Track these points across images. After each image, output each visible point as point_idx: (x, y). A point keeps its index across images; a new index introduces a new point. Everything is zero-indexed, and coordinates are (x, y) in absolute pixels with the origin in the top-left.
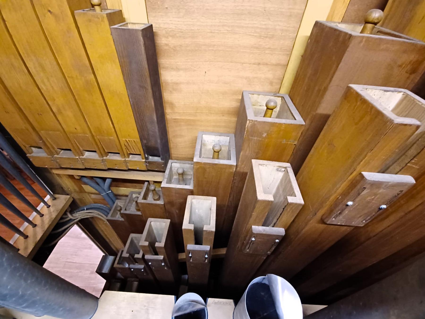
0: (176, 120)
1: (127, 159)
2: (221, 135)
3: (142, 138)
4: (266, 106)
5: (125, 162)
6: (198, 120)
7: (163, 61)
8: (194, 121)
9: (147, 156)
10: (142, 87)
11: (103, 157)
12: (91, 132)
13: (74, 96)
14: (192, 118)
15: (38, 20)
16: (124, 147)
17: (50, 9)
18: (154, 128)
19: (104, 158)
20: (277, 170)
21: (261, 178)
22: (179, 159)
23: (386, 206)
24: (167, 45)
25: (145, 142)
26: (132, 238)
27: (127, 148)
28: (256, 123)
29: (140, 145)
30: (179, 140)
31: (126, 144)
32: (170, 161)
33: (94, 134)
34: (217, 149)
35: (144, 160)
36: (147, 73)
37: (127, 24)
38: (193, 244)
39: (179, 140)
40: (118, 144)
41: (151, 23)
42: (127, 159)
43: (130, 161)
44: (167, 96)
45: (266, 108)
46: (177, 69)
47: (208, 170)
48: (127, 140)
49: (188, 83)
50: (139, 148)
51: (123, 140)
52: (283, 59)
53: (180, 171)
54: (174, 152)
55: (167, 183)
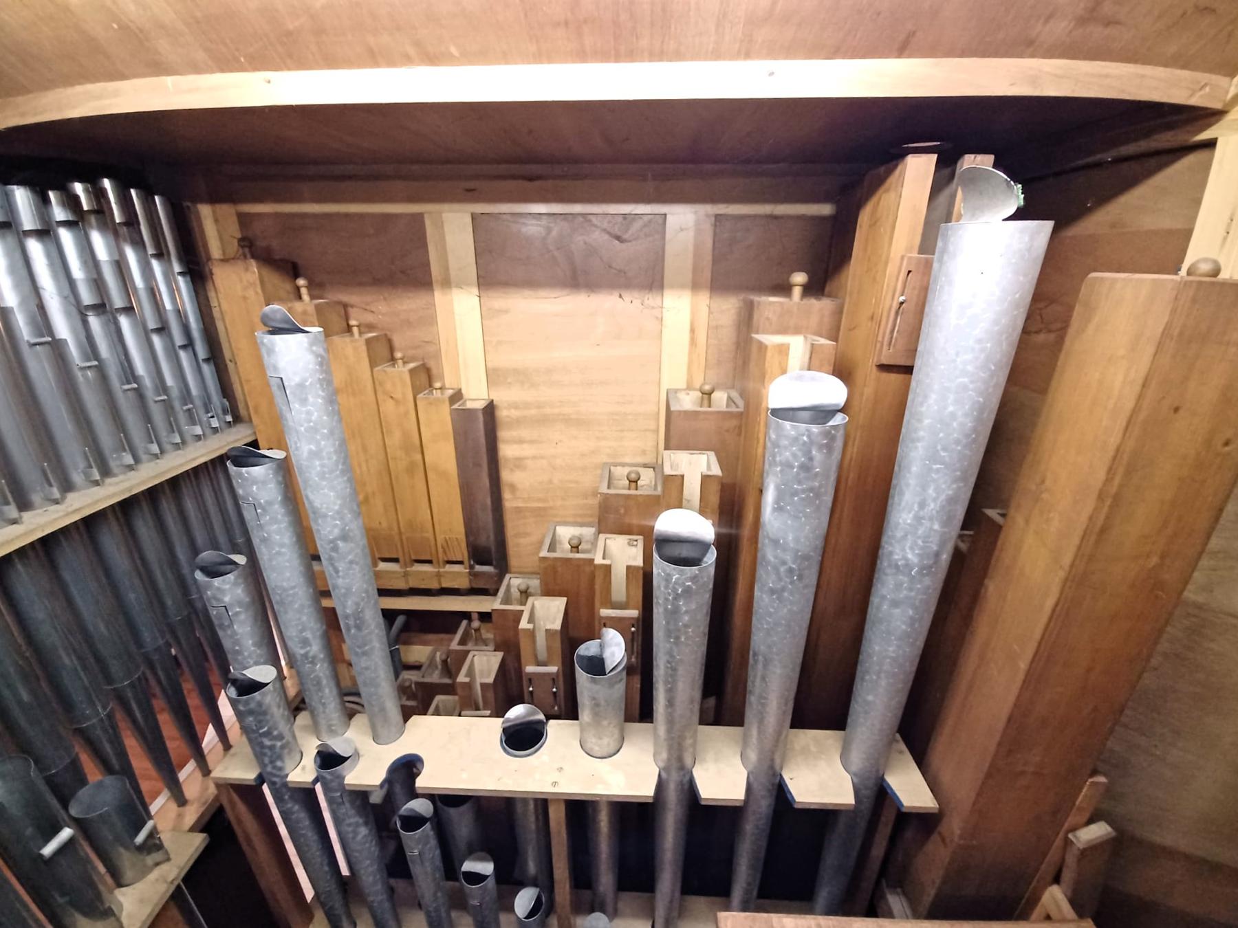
0: (519, 510)
1: (442, 570)
2: (582, 525)
3: (468, 533)
4: (628, 479)
5: (439, 575)
6: (551, 508)
7: (503, 434)
8: (544, 509)
9: (472, 563)
10: (478, 465)
11: (406, 567)
12: (399, 528)
13: (391, 479)
14: (540, 505)
15: (976, 597)
16: (440, 550)
17: (392, 395)
18: (486, 518)
19: (408, 569)
20: (629, 544)
21: (366, 310)
22: (522, 573)
23: (92, 228)
24: (508, 417)
25: (471, 539)
26: (438, 702)
27: (445, 552)
28: (608, 496)
29: (464, 545)
30: (523, 541)
31: (445, 545)
32: (508, 576)
33: (403, 530)
34: (575, 542)
35: (467, 571)
36: (484, 449)
37: (466, 401)
38: (532, 665)
39: (523, 541)
40: (433, 542)
41: (491, 398)
42: (442, 570)
43: (446, 572)
44: (506, 475)
45: (628, 482)
46: (521, 441)
47: (559, 569)
48: (447, 537)
49: (534, 458)
50: (462, 552)
51: (440, 539)
52: (653, 426)
53: (523, 587)
54: (514, 561)
55: (501, 604)
